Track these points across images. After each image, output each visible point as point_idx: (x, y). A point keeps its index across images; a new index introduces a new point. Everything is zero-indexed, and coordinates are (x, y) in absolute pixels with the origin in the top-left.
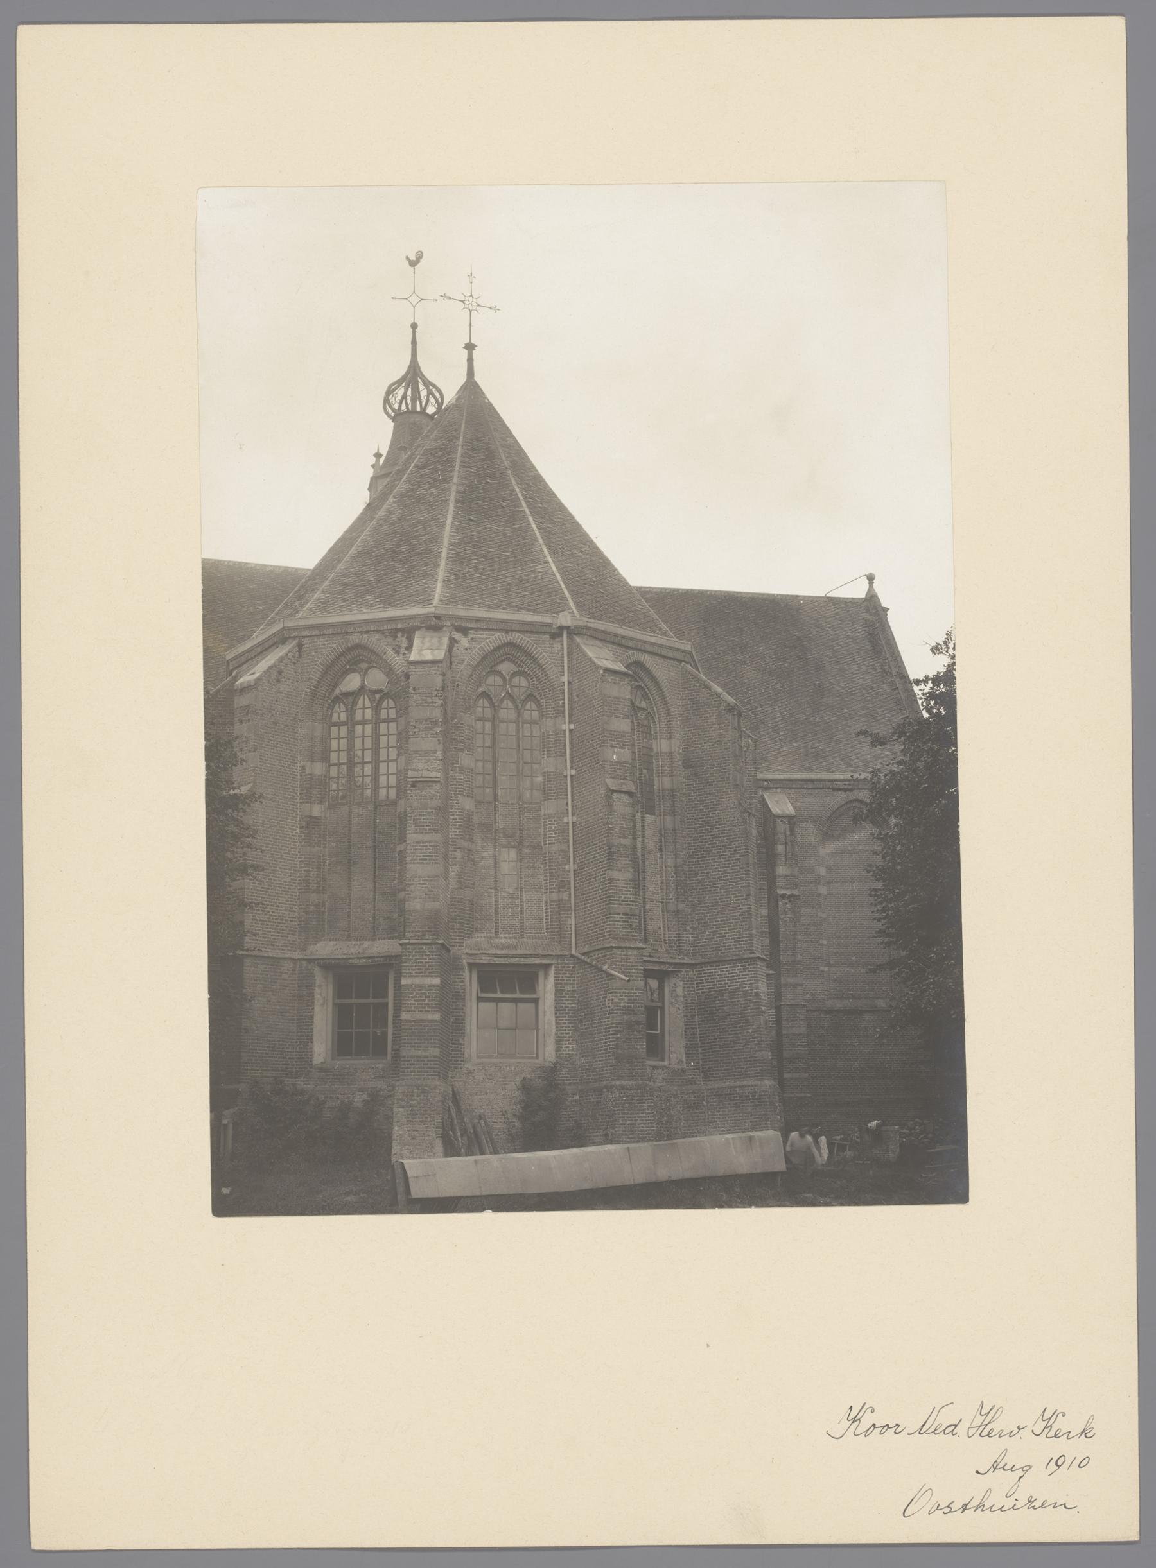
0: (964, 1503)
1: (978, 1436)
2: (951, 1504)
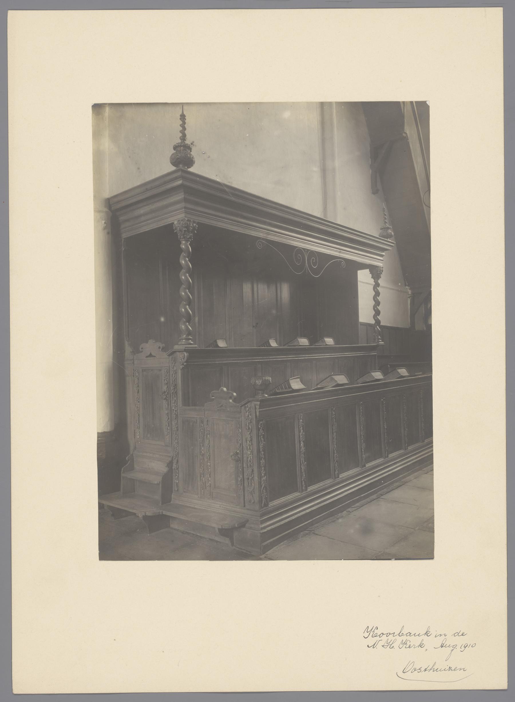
0: (425, 668)
1: (405, 648)
2: (420, 668)
